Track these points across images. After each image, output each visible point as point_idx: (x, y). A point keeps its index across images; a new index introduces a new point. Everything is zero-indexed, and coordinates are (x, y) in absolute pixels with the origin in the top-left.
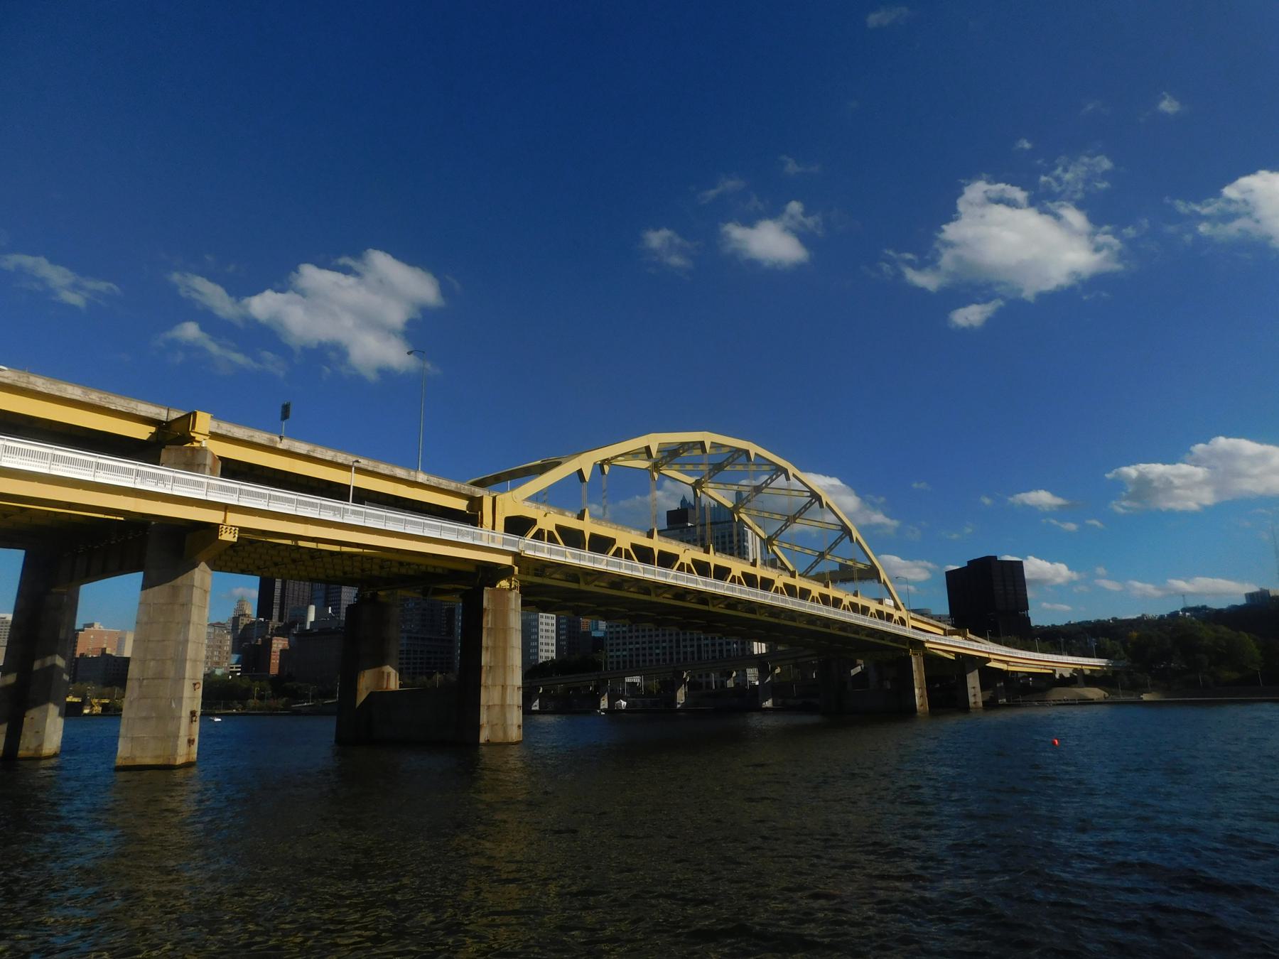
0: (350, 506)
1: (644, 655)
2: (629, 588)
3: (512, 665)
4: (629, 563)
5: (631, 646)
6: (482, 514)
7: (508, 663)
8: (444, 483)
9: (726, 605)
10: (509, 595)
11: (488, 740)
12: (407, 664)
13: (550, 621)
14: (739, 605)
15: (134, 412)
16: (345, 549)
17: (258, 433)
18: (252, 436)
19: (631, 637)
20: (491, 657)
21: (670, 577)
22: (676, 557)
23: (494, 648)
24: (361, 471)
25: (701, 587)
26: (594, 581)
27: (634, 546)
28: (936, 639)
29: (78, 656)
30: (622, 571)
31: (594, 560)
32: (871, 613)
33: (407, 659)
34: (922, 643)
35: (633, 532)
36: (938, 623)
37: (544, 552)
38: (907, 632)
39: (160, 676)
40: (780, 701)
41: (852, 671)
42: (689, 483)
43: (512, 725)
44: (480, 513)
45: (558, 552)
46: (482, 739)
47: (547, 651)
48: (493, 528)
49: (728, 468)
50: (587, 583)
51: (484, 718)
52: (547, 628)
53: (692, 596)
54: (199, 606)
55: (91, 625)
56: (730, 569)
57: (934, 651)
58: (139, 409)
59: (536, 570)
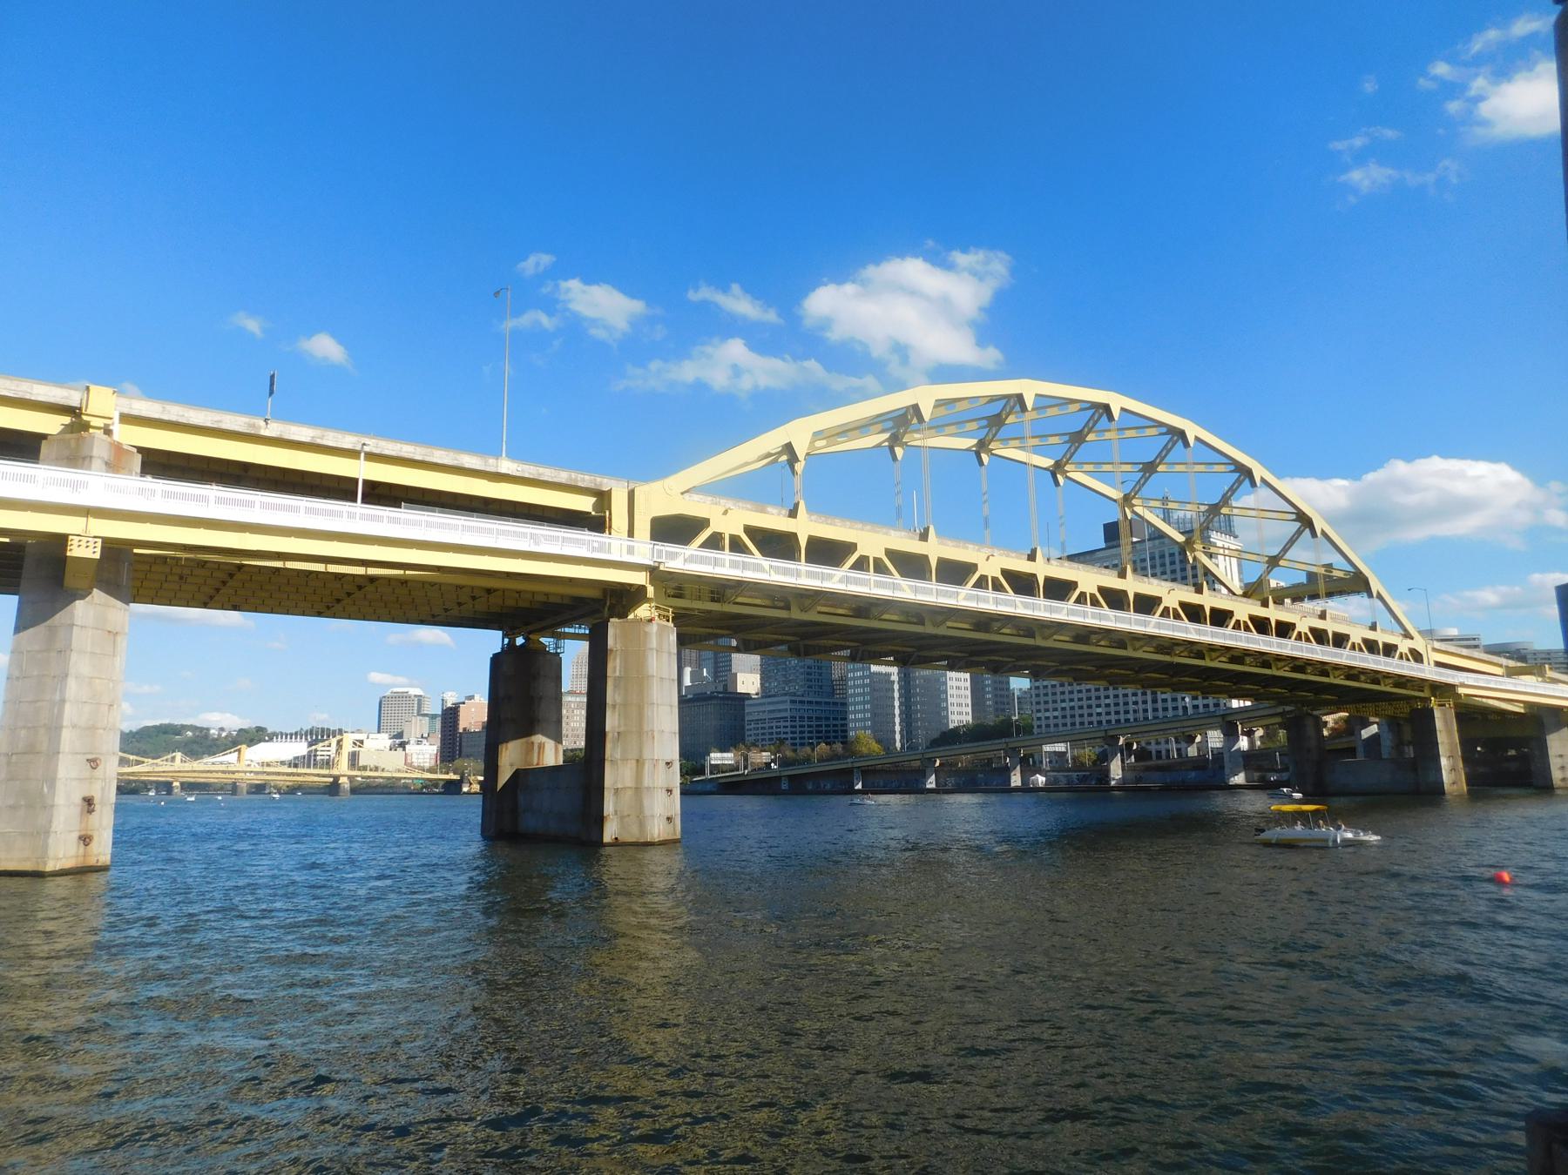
0: (359, 508)
1: (1081, 716)
2: (1099, 642)
3: (653, 731)
4: (1096, 610)
5: (1064, 705)
6: (610, 514)
7: (646, 728)
8: (547, 474)
9: (1156, 648)
10: (647, 629)
11: (616, 839)
12: (792, 733)
13: (962, 684)
14: (1093, 636)
15: (28, 397)
16: (372, 571)
17: (229, 417)
18: (220, 421)
19: (1063, 693)
20: (619, 720)
21: (1151, 625)
22: (1158, 601)
23: (625, 705)
24: (372, 457)
25: (1193, 637)
26: (1142, 647)
27: (1102, 590)
28: (1489, 682)
29: (461, 731)
30: (1087, 621)
31: (1051, 610)
32: (1401, 654)
33: (792, 727)
34: (1452, 687)
35: (892, 532)
36: (1490, 656)
37: (988, 602)
38: (1428, 672)
39: (31, 750)
40: (1256, 775)
41: (1363, 732)
42: (1045, 466)
43: (653, 816)
44: (607, 513)
45: (1006, 603)
46: (607, 838)
47: (960, 713)
48: (631, 533)
49: (1091, 437)
50: (1045, 638)
51: (609, 807)
52: (958, 684)
53: (1181, 649)
54: (92, 653)
55: (471, 698)
56: (1295, 624)
57: (1484, 700)
58: (35, 392)
59: (712, 592)
